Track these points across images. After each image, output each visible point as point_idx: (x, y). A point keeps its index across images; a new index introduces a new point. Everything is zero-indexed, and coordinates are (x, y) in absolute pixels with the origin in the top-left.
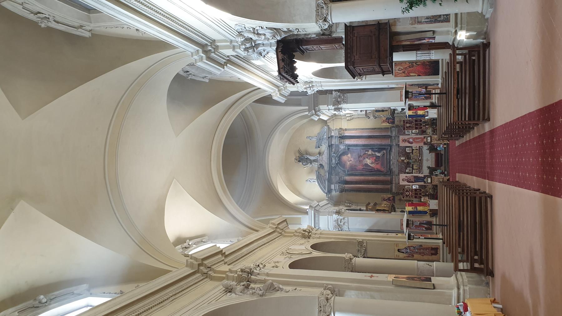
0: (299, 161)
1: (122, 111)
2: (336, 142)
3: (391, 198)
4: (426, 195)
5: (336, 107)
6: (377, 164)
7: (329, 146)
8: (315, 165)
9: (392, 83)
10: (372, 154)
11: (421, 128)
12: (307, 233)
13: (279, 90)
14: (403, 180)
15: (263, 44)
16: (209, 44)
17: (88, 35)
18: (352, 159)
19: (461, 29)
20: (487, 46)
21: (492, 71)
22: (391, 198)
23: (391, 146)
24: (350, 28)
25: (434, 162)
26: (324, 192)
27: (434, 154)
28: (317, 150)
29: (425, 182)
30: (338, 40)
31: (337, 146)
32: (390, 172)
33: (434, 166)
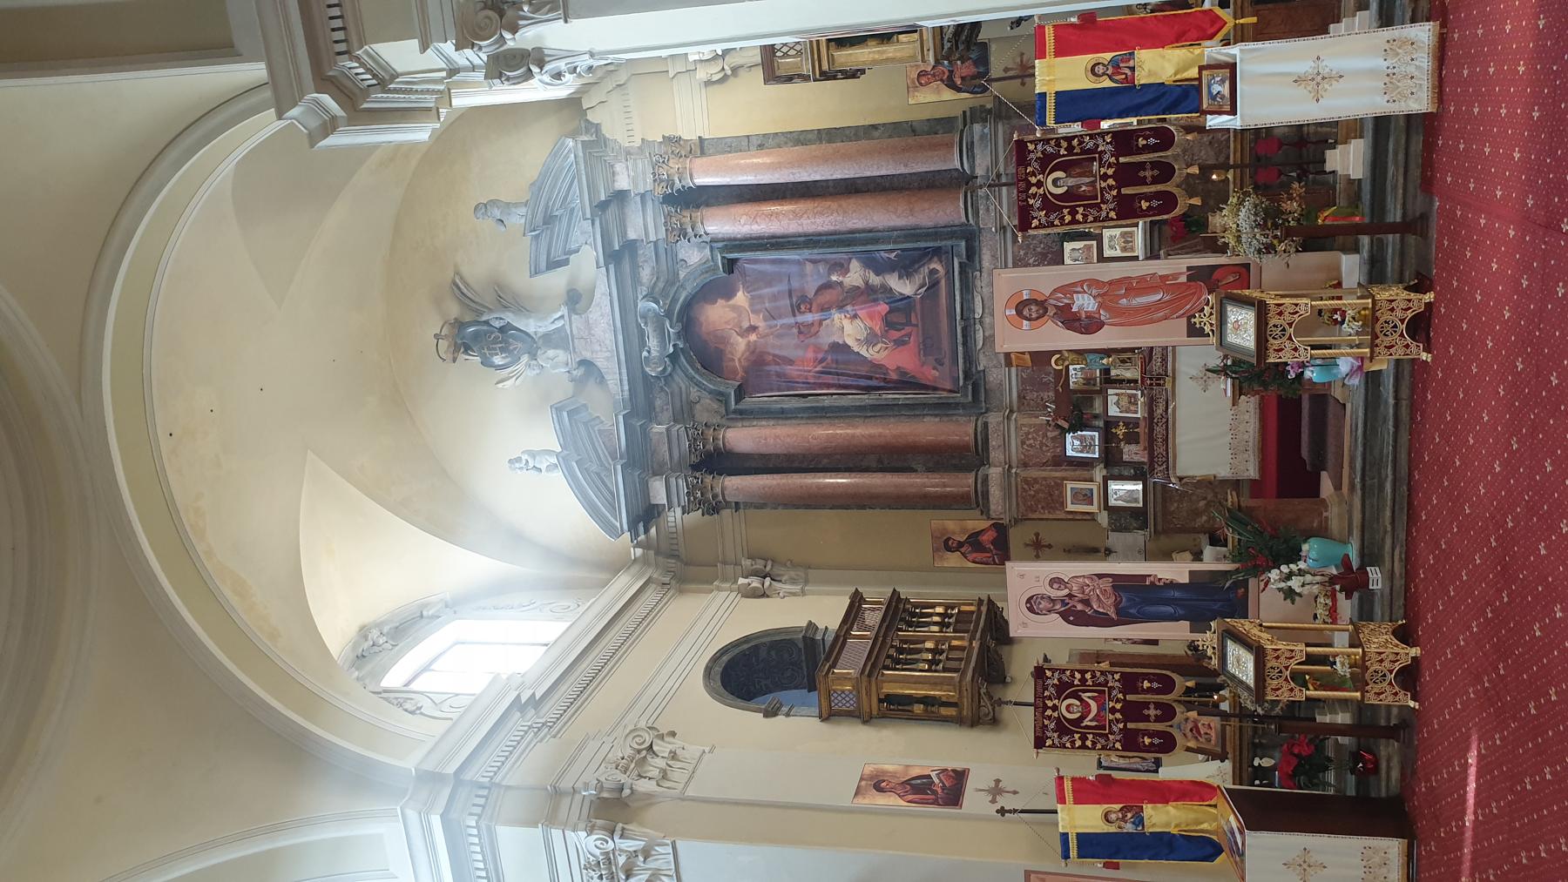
3: (986, 538)
6: (900, 343)
8: (556, 361)
11: (1169, 201)
14: (1032, 605)
22: (986, 538)
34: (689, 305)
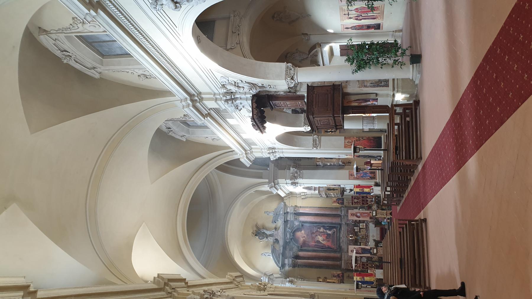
0: (256, 235)
1: (111, 146)
2: (290, 217)
3: (340, 275)
4: (372, 267)
5: (293, 181)
6: (328, 241)
7: (285, 222)
8: (271, 240)
9: (342, 153)
10: (324, 232)
12: (262, 286)
13: (246, 154)
15: (241, 98)
16: (196, 95)
17: (97, 76)
18: (305, 236)
19: (398, 92)
20: (417, 103)
21: (421, 120)
22: (340, 275)
23: (340, 225)
24: (311, 88)
25: (379, 236)
26: (278, 265)
27: (379, 228)
28: (274, 225)
29: (371, 253)
30: (301, 97)
31: (292, 222)
32: (339, 249)
33: (379, 239)
34: (295, 231)
